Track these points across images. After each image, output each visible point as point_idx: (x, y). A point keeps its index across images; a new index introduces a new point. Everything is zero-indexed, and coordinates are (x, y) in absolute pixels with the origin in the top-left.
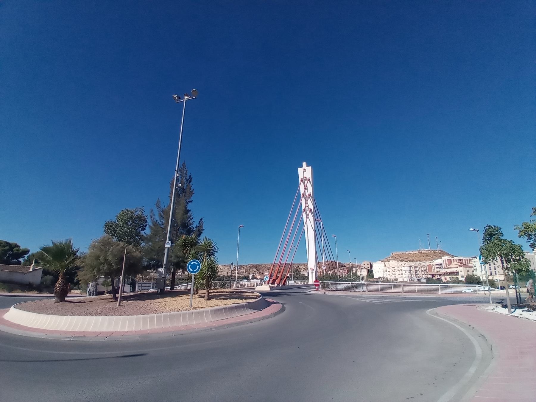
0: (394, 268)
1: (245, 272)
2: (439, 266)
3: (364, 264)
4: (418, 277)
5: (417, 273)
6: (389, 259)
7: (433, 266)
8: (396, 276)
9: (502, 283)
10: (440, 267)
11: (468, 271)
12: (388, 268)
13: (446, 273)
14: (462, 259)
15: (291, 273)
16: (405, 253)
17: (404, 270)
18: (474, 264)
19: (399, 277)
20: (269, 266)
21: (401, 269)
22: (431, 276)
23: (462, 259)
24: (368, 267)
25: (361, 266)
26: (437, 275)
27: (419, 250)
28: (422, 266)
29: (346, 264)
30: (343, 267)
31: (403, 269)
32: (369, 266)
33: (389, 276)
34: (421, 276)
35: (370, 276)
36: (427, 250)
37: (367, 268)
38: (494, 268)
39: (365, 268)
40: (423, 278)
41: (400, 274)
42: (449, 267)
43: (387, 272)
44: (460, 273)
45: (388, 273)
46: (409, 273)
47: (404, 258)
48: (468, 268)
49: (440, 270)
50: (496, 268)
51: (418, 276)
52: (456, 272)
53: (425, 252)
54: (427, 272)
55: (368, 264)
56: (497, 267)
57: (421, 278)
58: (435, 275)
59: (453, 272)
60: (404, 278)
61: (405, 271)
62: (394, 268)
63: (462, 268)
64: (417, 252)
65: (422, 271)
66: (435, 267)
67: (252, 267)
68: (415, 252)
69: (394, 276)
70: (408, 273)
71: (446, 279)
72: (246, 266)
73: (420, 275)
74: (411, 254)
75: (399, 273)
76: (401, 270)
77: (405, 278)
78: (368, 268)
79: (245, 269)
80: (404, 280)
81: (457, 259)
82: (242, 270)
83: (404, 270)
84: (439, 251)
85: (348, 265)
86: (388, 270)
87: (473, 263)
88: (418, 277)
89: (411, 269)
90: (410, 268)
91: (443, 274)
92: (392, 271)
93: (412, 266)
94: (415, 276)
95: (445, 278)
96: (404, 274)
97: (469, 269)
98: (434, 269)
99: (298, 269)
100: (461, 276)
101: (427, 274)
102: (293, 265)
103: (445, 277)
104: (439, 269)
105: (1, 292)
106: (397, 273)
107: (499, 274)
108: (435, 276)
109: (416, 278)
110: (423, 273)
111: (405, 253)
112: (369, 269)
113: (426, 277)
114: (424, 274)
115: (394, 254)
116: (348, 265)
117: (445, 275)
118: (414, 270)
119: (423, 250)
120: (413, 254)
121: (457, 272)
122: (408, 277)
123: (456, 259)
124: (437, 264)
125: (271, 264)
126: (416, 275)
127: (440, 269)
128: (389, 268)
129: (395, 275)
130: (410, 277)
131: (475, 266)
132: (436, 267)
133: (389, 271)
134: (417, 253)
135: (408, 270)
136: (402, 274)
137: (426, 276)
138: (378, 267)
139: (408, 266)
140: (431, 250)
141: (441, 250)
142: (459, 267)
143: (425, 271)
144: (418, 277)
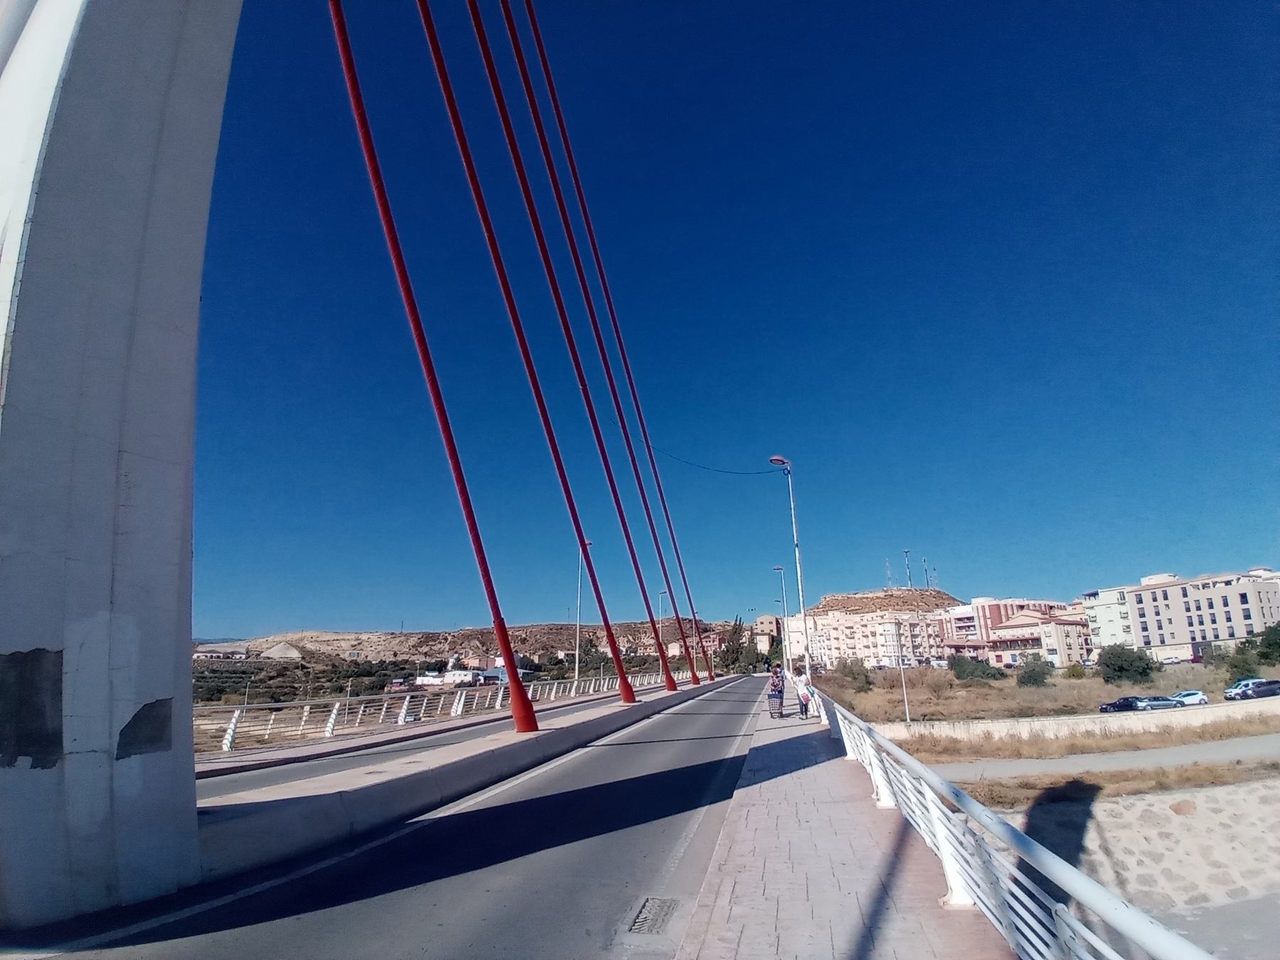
0: (852, 628)
1: (447, 649)
2: (966, 623)
3: (762, 623)
4: (918, 654)
5: (917, 644)
6: (816, 610)
7: (949, 624)
8: (857, 651)
9: (1193, 668)
10: (969, 627)
11: (1067, 636)
12: (834, 629)
13: (1000, 642)
14: (1028, 605)
15: (575, 650)
16: (853, 596)
17: (881, 635)
18: (1092, 613)
19: (867, 654)
20: (517, 634)
21: (873, 630)
22: (953, 651)
23: (1028, 605)
24: (772, 631)
25: (755, 627)
26: (966, 649)
27: (885, 589)
28: (929, 622)
29: (714, 625)
30: (707, 631)
31: (879, 629)
32: (774, 627)
33: (837, 651)
34: (927, 650)
35: (777, 652)
36: (904, 588)
37: (769, 631)
38: (1241, 614)
39: (763, 634)
40: (933, 656)
41: (868, 647)
42: (1008, 623)
43: (832, 639)
44: (1044, 641)
45: (834, 644)
46: (896, 643)
47: (853, 608)
48: (1066, 626)
49: (967, 635)
50: (1165, 624)
51: (918, 651)
52: (1033, 640)
53: (900, 593)
54: (942, 641)
55: (771, 623)
56: (1167, 622)
57: (926, 655)
58: (964, 647)
59: (1021, 637)
60: (880, 656)
61: (883, 637)
62: (852, 628)
63: (1051, 627)
64: (882, 594)
65: (930, 636)
66: (954, 625)
67: (468, 637)
68: (878, 595)
69: (850, 651)
70: (892, 641)
71: (999, 658)
72: (452, 634)
73: (925, 648)
74: (867, 598)
75: (866, 644)
76: (874, 634)
77: (884, 656)
78: (772, 633)
79: (448, 642)
80: (882, 664)
81: (1014, 605)
82: (439, 646)
83: (881, 635)
84: (933, 593)
85: (719, 627)
86: (834, 634)
87: (1088, 612)
88: (918, 654)
89: (901, 632)
90: (899, 629)
91: (991, 644)
92: (844, 637)
93: (904, 624)
94: (910, 650)
95: (997, 656)
96: (883, 646)
97: (1069, 628)
98: (950, 631)
99: (594, 638)
100: (1049, 650)
101: (942, 645)
102: (580, 629)
103: (998, 653)
104: (964, 632)
105: (1276, 716)
106: (860, 642)
107: (1174, 642)
108: (961, 650)
109: (915, 656)
110: (932, 641)
111: (853, 596)
112: (775, 633)
113: (940, 654)
114: (935, 645)
115: (828, 599)
116: (719, 627)
117: (997, 647)
118: (909, 633)
119: (895, 588)
120: (872, 599)
121: (1032, 637)
122: (893, 654)
123: (1012, 605)
124: (959, 619)
125: (521, 627)
126: (915, 647)
127: (968, 633)
128: (836, 629)
129: (855, 648)
130: (897, 654)
131: (1095, 621)
132: (957, 627)
133: (837, 639)
134: (881, 596)
135: (893, 635)
136: (875, 646)
137: (940, 650)
138: (798, 628)
139: (894, 621)
140: (913, 589)
141: (937, 589)
142: (1043, 623)
143: (937, 636)
144: (920, 653)
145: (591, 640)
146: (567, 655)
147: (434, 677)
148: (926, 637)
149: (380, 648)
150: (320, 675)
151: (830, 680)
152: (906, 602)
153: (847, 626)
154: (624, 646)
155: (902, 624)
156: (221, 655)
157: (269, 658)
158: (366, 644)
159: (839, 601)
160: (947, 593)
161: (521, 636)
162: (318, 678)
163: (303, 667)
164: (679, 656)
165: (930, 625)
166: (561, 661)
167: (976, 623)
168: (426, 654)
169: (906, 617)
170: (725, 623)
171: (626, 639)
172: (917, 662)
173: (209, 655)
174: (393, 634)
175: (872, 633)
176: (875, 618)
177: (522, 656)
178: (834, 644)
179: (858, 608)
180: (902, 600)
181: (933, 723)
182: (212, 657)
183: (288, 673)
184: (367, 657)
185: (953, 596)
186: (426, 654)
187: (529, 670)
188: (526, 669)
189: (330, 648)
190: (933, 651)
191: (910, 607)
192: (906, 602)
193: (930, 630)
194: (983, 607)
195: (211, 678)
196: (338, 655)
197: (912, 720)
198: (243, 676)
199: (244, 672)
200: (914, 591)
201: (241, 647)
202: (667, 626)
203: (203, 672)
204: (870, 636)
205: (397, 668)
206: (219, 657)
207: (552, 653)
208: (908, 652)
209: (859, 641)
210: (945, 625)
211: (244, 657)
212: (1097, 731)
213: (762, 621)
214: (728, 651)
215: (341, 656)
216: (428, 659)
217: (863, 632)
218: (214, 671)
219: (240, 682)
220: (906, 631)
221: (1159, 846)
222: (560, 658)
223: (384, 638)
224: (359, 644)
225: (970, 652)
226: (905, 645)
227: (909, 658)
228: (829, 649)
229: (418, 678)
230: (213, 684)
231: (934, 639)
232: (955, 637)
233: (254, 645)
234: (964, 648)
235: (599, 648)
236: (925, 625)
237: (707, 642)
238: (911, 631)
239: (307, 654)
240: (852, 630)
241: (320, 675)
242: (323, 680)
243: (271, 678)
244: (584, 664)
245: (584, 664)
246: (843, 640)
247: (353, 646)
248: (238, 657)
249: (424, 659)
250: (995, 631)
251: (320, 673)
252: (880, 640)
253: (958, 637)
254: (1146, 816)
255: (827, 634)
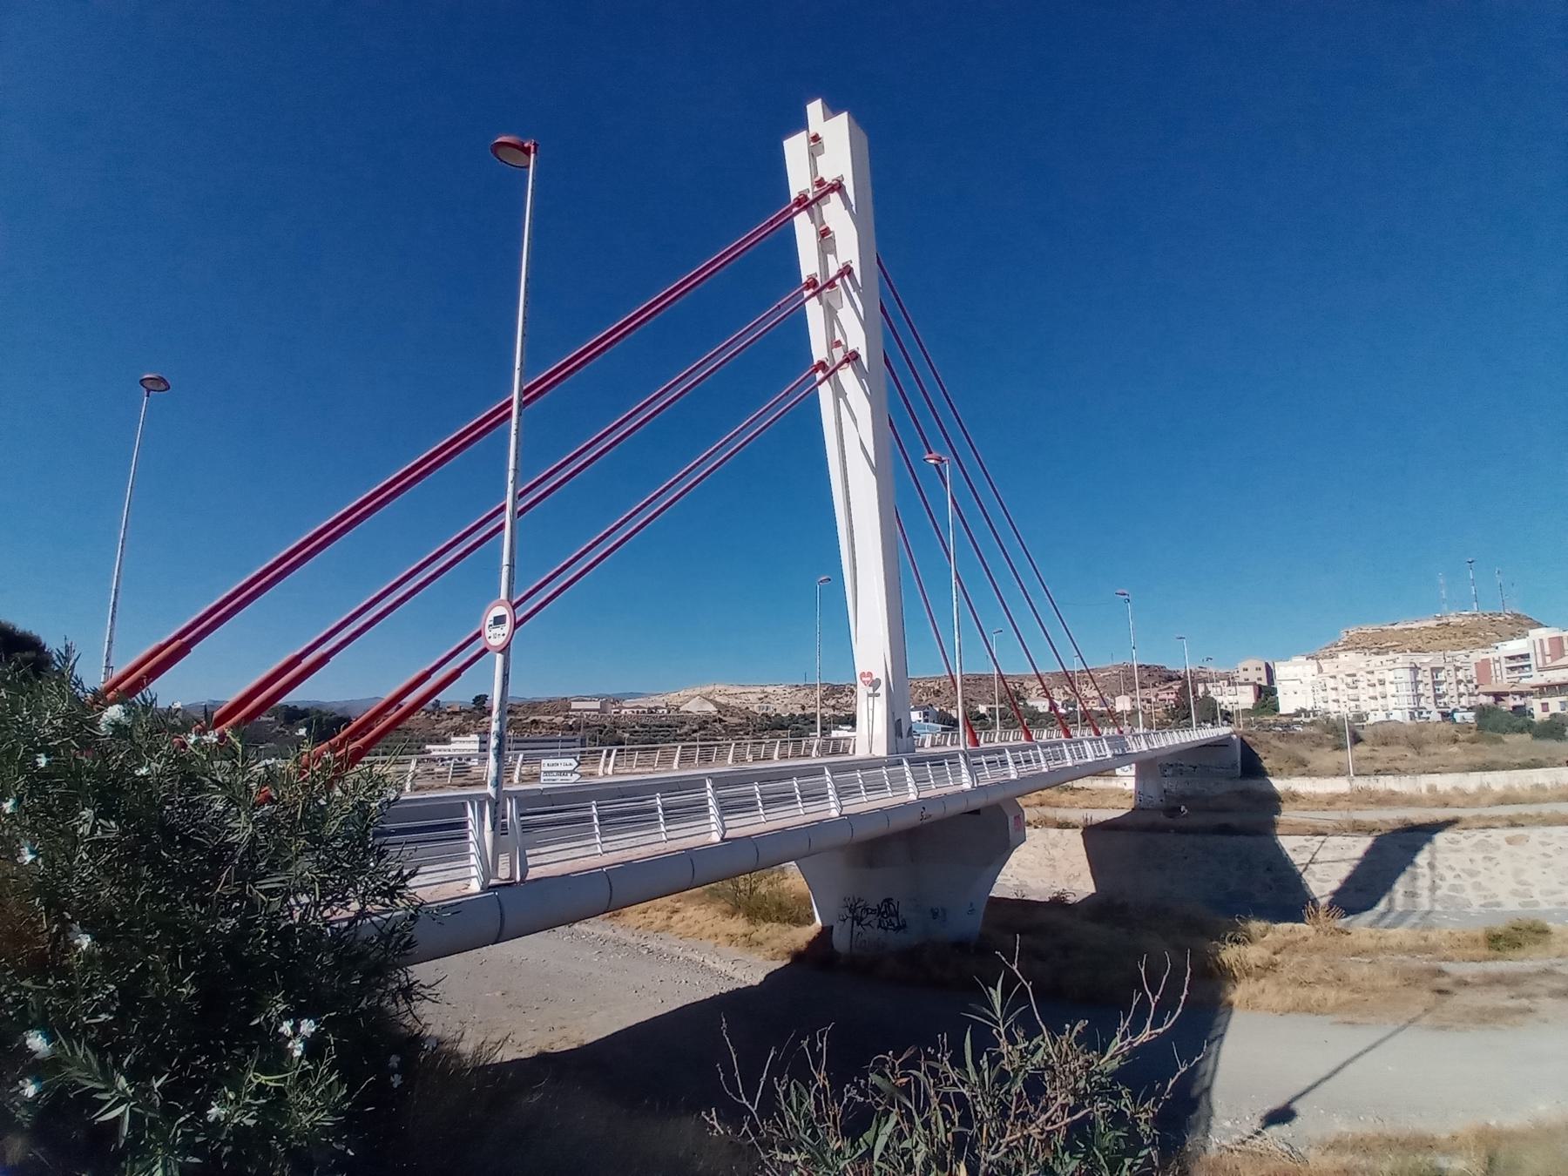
0: (1354, 675)
2: (1519, 662)
4: (1442, 705)
5: (1441, 692)
6: (1334, 649)
10: (1523, 667)
17: (1392, 683)
19: (1373, 707)
20: (929, 685)
21: (1381, 677)
24: (1260, 679)
26: (1511, 696)
28: (1458, 664)
31: (1389, 676)
32: (1263, 674)
41: (1375, 698)
45: (1333, 695)
46: (1410, 693)
47: (1388, 644)
49: (1521, 678)
51: (1442, 700)
53: (1459, 620)
57: (1453, 706)
58: (1507, 694)
60: (1390, 708)
64: (1432, 623)
65: (1459, 682)
66: (1504, 666)
68: (1426, 624)
69: (1353, 704)
70: (1406, 690)
71: (1545, 707)
75: (1372, 694)
76: (1382, 683)
77: (1395, 709)
78: (1259, 682)
80: (1392, 718)
83: (1392, 683)
84: (1509, 617)
88: (1442, 705)
89: (1419, 678)
90: (1416, 675)
92: (1344, 687)
94: (1431, 700)
95: (1543, 704)
98: (1498, 673)
99: (1022, 690)
103: (1544, 700)
104: (1516, 673)
106: (1364, 693)
108: (1503, 698)
111: (1390, 627)
112: (1264, 683)
114: (1466, 693)
115: (1351, 633)
117: (1544, 693)
118: (1430, 681)
120: (1418, 630)
124: (1512, 658)
126: (1437, 697)
129: (1358, 700)
130: (1412, 706)
132: (1508, 668)
134: (1432, 626)
137: (1473, 699)
139: (1408, 665)
141: (1516, 612)
144: (1445, 704)
145: (1018, 692)
146: (990, 709)
147: (849, 731)
148: (1455, 683)
149: (786, 701)
150: (738, 728)
151: (1304, 738)
152: (1468, 633)
153: (1347, 673)
154: (1060, 700)
155: (1420, 669)
156: (646, 710)
157: (688, 712)
158: (773, 697)
159: (1369, 635)
160: (1529, 616)
161: (933, 688)
162: (736, 731)
163: (721, 721)
164: (1131, 711)
165: (1461, 668)
166: (983, 717)
167: (1532, 661)
168: (834, 707)
169: (1426, 660)
170: (1199, 669)
171: (1061, 691)
172: (1440, 715)
173: (635, 710)
174: (797, 686)
175: (1380, 681)
176: (1384, 663)
177: (937, 710)
178: (1333, 695)
179: (1396, 643)
180: (1462, 629)
181: (1378, 777)
182: (638, 712)
183: (709, 726)
184: (775, 710)
185: (1538, 621)
186: (834, 707)
187: (949, 725)
188: (944, 724)
189: (738, 701)
190: (1464, 701)
191: (1473, 639)
192: (1468, 633)
193: (1461, 675)
194: (1541, 640)
195: (642, 732)
196: (747, 708)
197: (1356, 775)
198: (670, 729)
199: (669, 726)
200: (1481, 616)
201: (658, 701)
202: (1115, 675)
203: (634, 727)
204: (1377, 684)
205: (807, 721)
206: (644, 712)
207: (971, 706)
208: (1427, 703)
209: (1363, 692)
210: (1492, 666)
211: (666, 711)
212: (1548, 785)
213: (1246, 667)
214: (1177, 707)
215: (751, 709)
216: (836, 713)
217: (1369, 680)
218: (643, 726)
219: (669, 735)
220: (1425, 677)
221: (1480, 865)
222: (981, 712)
223: (789, 691)
224: (766, 697)
225: (1515, 699)
226: (1423, 695)
227: (1429, 710)
228: (1325, 702)
229: (833, 732)
230: (647, 737)
231: (1466, 686)
232: (1502, 680)
233: (673, 698)
234: (1508, 695)
235: (1028, 702)
236: (1453, 669)
237: (1168, 694)
238: (1433, 677)
239: (722, 708)
240: (1355, 678)
241: (738, 728)
242: (742, 733)
243: (695, 731)
244: (1011, 720)
245: (1011, 720)
246: (1343, 690)
247: (760, 699)
248: (660, 711)
249: (832, 712)
250: (1542, 673)
251: (737, 726)
252: (1390, 689)
253: (1510, 680)
254: (1480, 845)
255: (1323, 684)
